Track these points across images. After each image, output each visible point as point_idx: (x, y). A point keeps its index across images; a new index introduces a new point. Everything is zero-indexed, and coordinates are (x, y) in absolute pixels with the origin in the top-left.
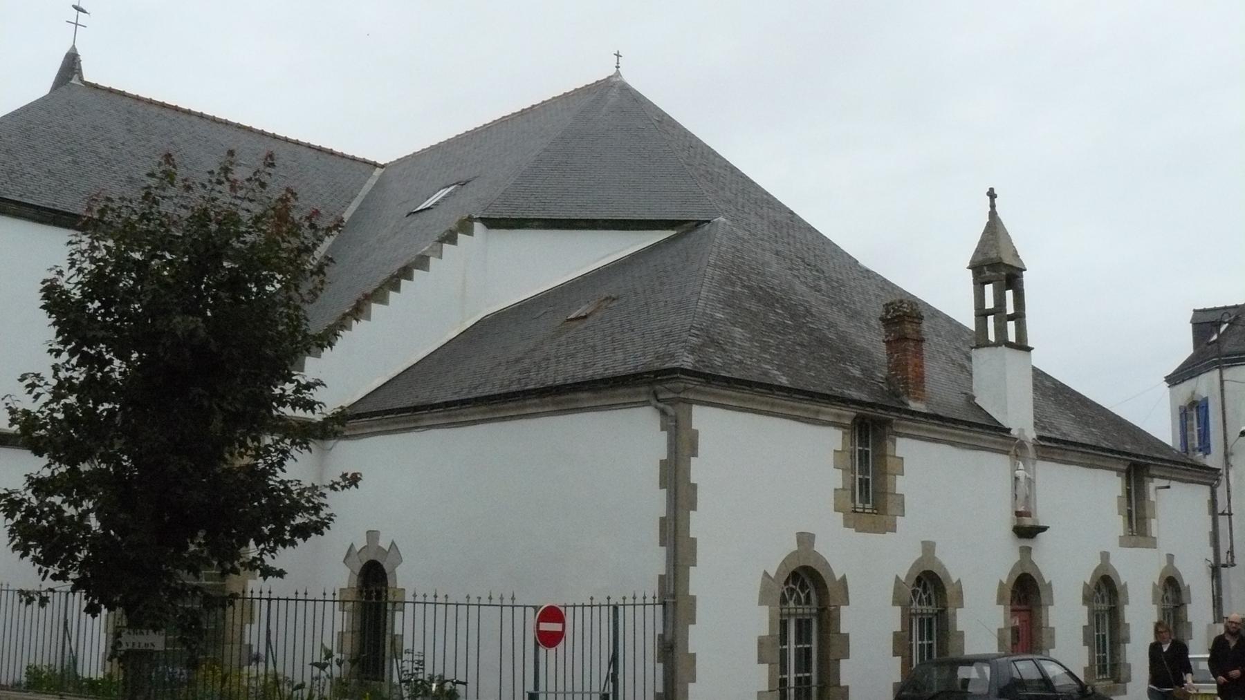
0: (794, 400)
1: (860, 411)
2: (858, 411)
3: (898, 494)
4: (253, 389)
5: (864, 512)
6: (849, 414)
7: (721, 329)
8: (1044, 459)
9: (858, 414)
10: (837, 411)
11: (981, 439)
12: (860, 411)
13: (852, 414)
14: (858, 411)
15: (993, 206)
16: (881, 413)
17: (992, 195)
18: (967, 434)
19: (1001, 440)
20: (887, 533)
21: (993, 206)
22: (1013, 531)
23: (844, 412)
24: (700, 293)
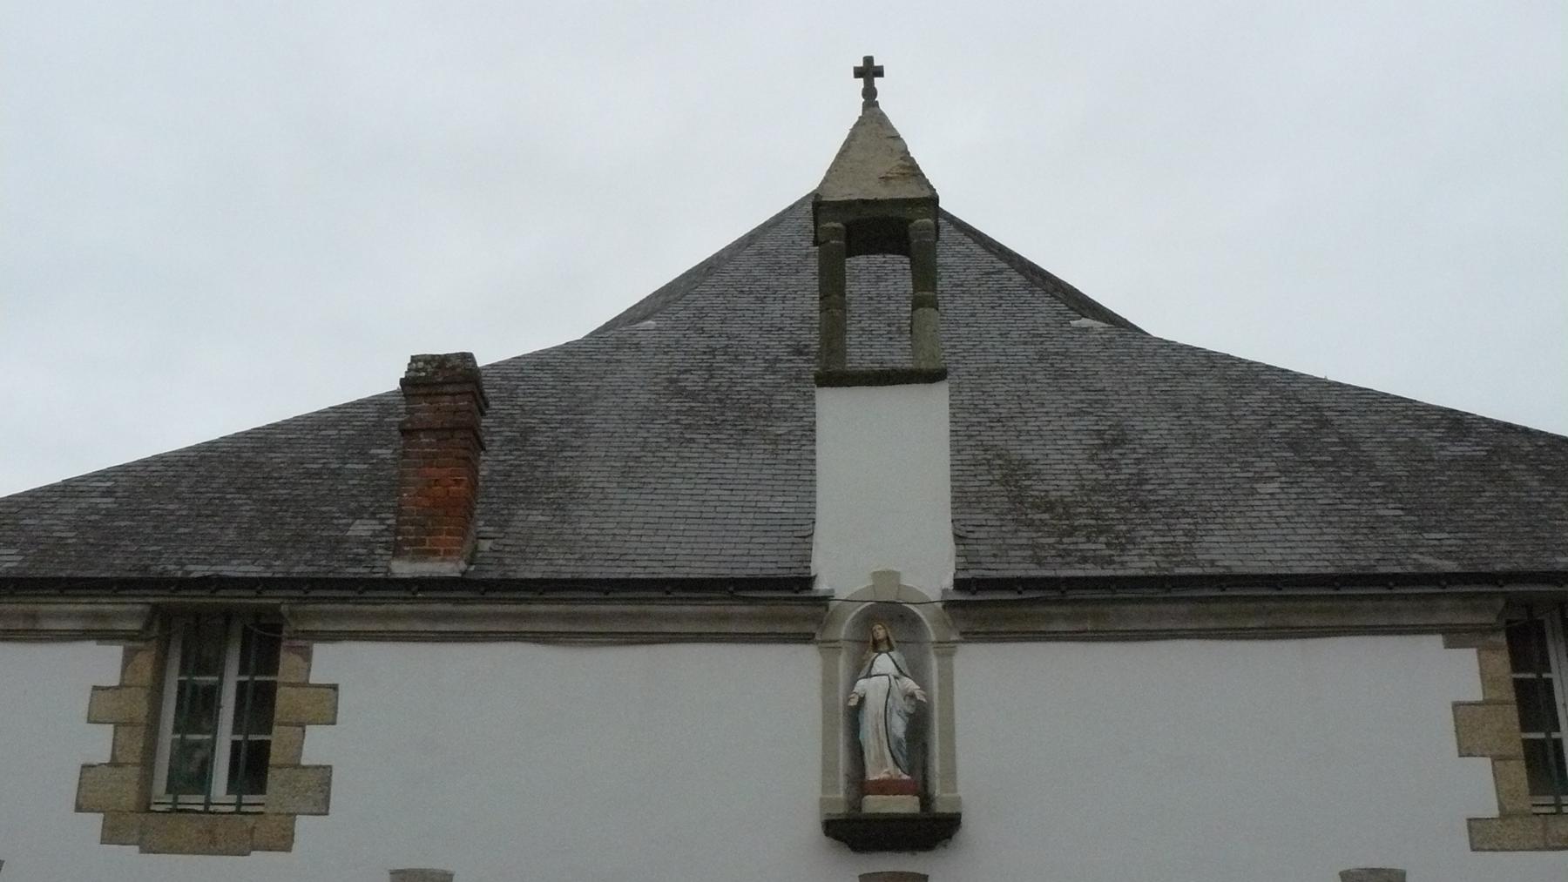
0: (675, 601)
1: (160, 600)
2: (152, 600)
3: (305, 768)
4: (1542, 707)
5: (206, 811)
6: (129, 612)
7: (54, 499)
8: (970, 636)
9: (156, 607)
10: (88, 607)
11: (647, 615)
12: (160, 600)
13: (139, 607)
14: (152, 600)
15: (870, 94)
16: (232, 597)
17: (869, 72)
18: (603, 608)
19: (745, 609)
20: (253, 853)
21: (870, 94)
22: (827, 834)
23: (107, 607)
24: (438, 440)
